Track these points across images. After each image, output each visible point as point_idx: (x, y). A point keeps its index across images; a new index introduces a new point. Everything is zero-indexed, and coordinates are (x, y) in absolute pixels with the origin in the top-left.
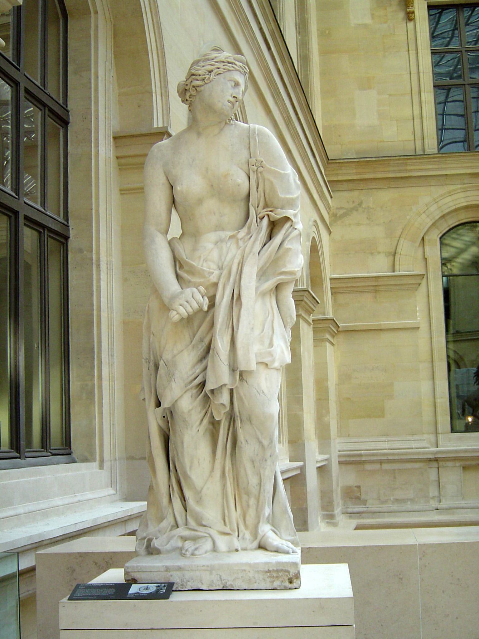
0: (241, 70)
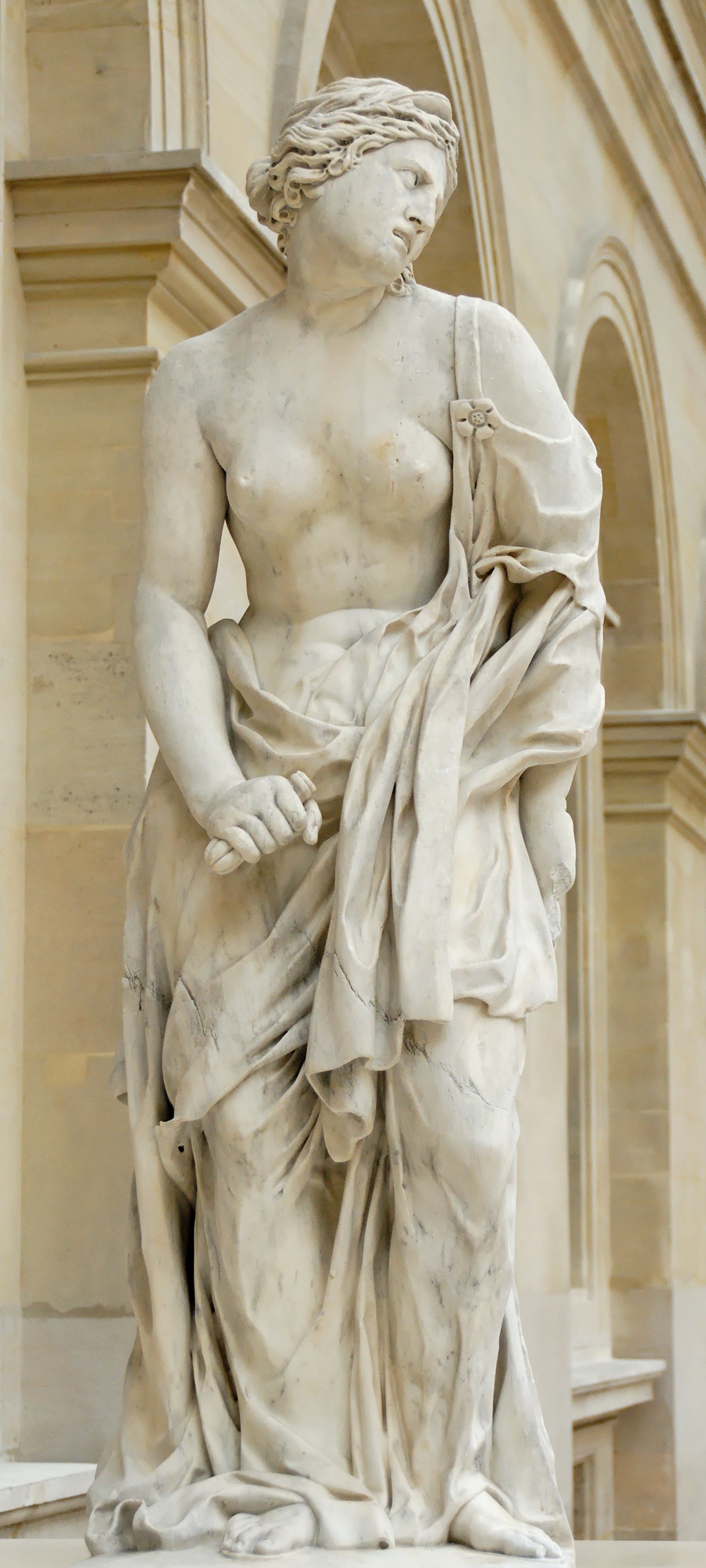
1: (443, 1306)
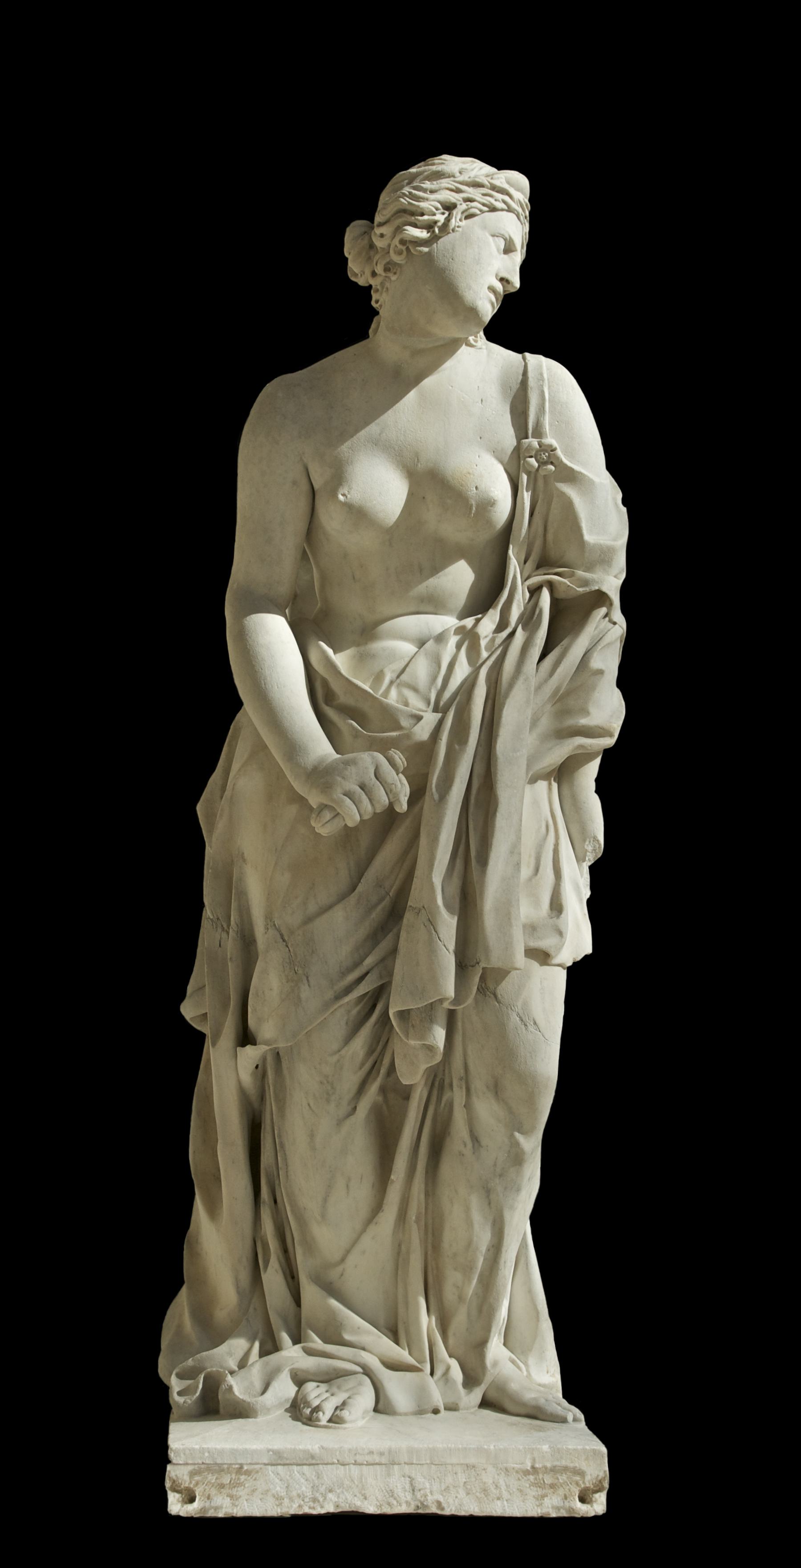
0: (520, 210)
1: (490, 1208)
